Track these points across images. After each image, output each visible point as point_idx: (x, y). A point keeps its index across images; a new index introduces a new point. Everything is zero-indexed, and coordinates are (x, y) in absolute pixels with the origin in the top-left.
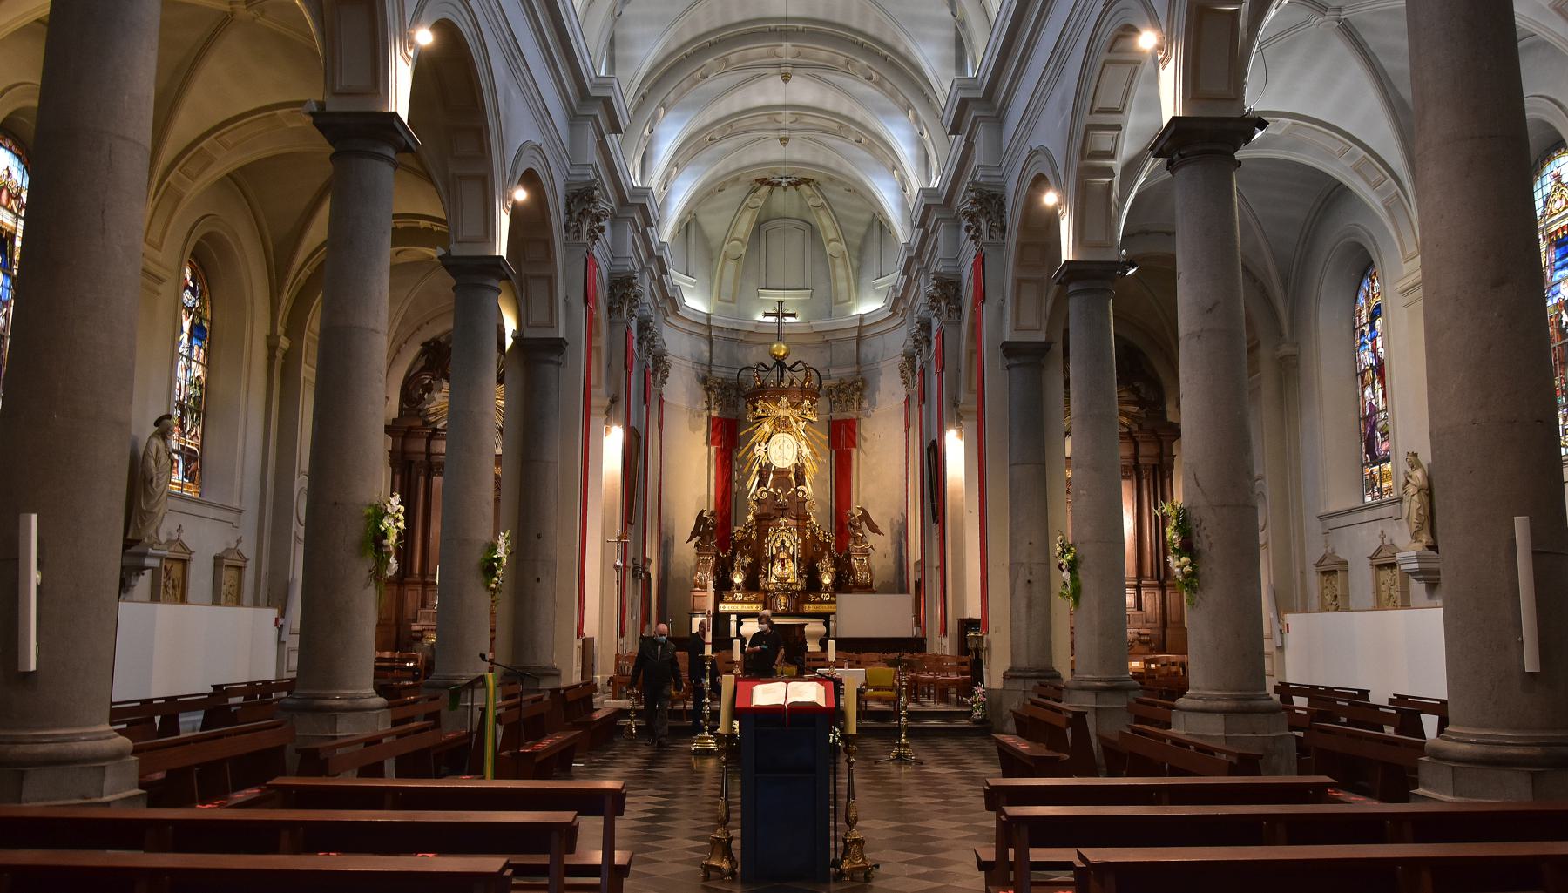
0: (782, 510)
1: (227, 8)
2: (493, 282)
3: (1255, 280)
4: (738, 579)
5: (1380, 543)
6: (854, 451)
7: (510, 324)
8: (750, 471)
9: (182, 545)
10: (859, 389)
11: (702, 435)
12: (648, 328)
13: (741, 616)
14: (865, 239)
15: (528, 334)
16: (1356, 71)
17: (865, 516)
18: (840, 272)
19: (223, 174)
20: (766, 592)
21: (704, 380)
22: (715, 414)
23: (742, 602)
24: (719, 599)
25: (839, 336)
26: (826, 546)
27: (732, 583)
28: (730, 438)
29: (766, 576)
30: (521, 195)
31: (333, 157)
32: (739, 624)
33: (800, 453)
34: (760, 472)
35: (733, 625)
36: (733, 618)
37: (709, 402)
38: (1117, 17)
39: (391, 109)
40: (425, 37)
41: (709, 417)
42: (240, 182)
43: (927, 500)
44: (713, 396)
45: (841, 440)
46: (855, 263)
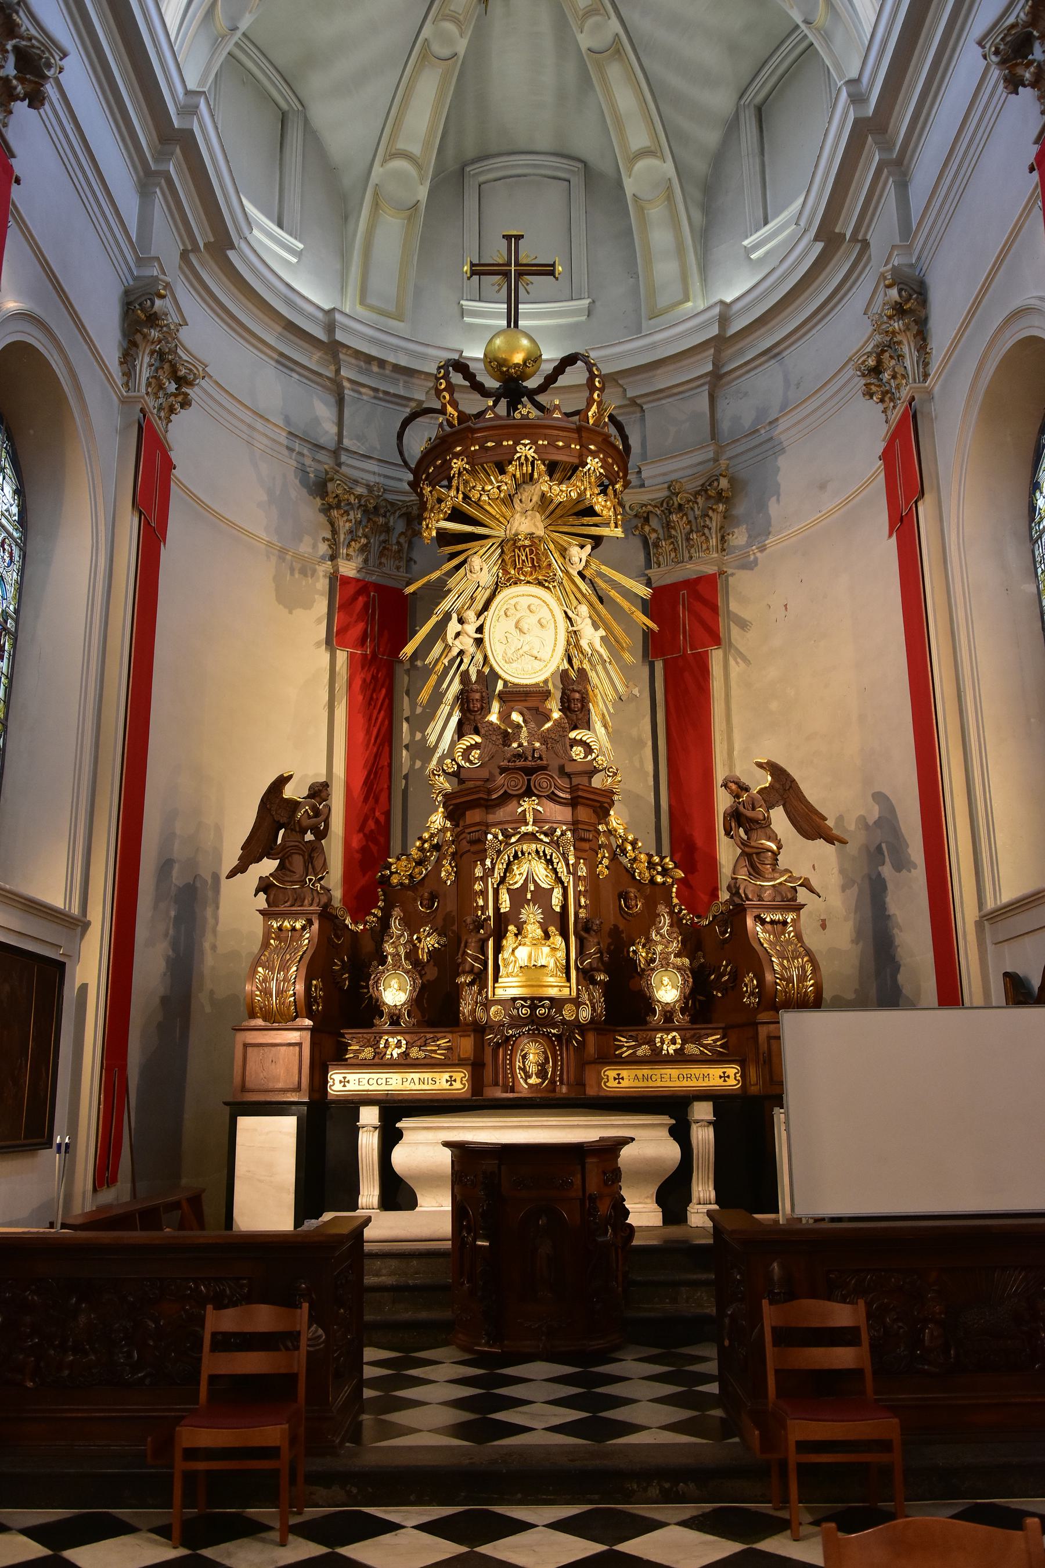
0: (528, 773)
4: (395, 993)
6: (716, 657)
8: (437, 697)
10: (720, 497)
11: (313, 619)
12: (153, 319)
13: (395, 1111)
14: (719, 160)
17: (783, 788)
18: (661, 238)
20: (479, 1029)
21: (320, 488)
22: (349, 569)
23: (405, 1063)
24: (328, 1052)
25: (663, 380)
26: (656, 894)
27: (375, 1007)
28: (382, 624)
29: (480, 978)
32: (390, 1137)
33: (574, 635)
34: (463, 699)
35: (368, 1142)
36: (369, 1116)
37: (333, 543)
41: (337, 581)
43: (428, 1104)
44: (344, 526)
45: (679, 638)
46: (697, 216)
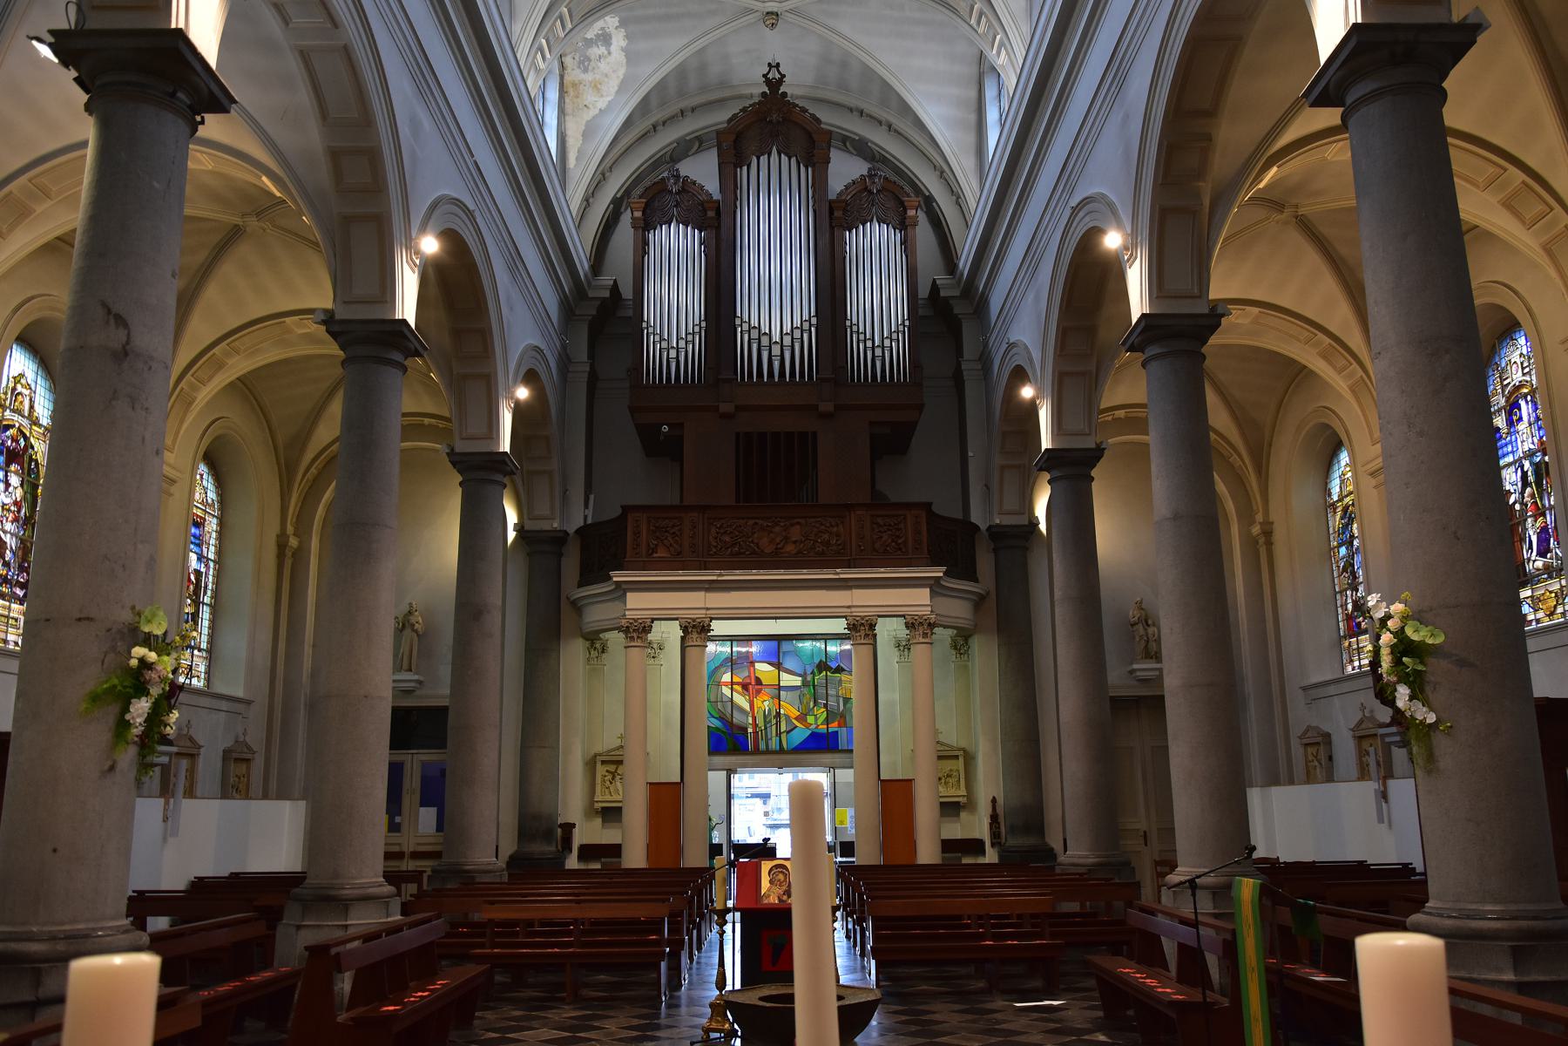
1: (238, 220)
2: (499, 477)
3: (851, 110)
5: (1360, 716)
7: (512, 517)
9: (191, 739)
15: (529, 526)
16: (1312, 257)
19: (233, 378)
30: (523, 393)
31: (343, 363)
38: (1087, 219)
39: (398, 316)
40: (430, 245)
42: (245, 388)
